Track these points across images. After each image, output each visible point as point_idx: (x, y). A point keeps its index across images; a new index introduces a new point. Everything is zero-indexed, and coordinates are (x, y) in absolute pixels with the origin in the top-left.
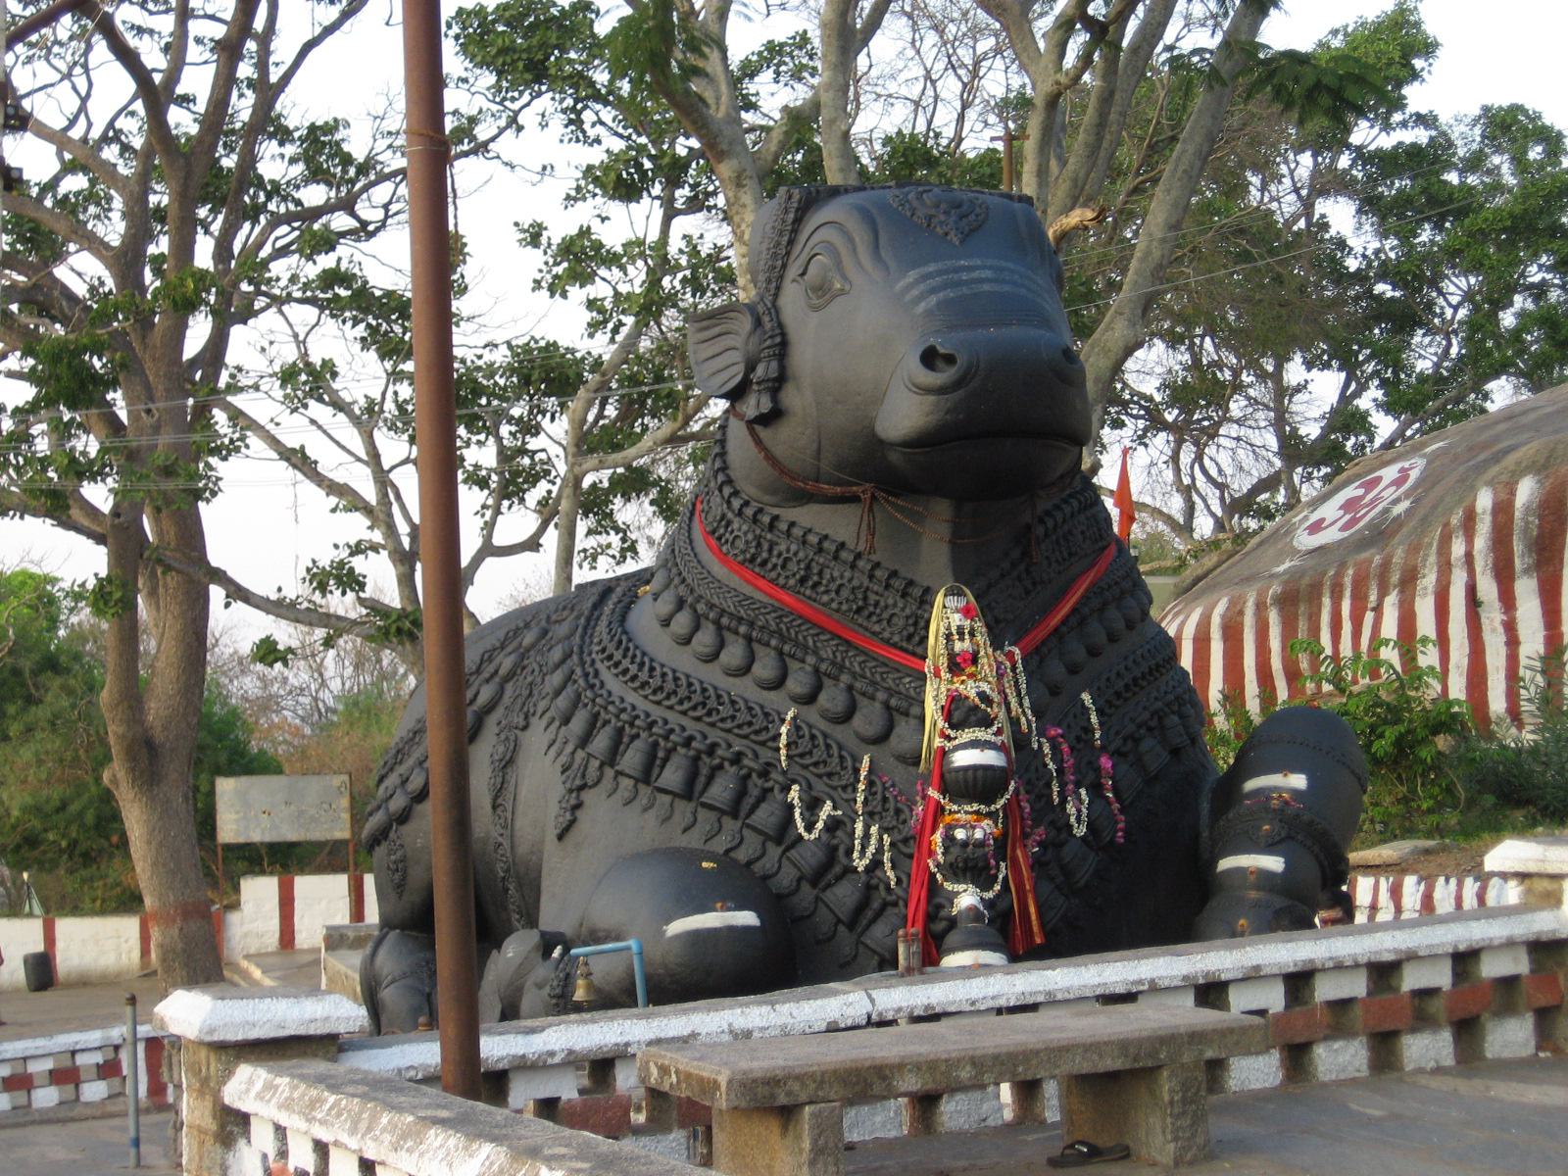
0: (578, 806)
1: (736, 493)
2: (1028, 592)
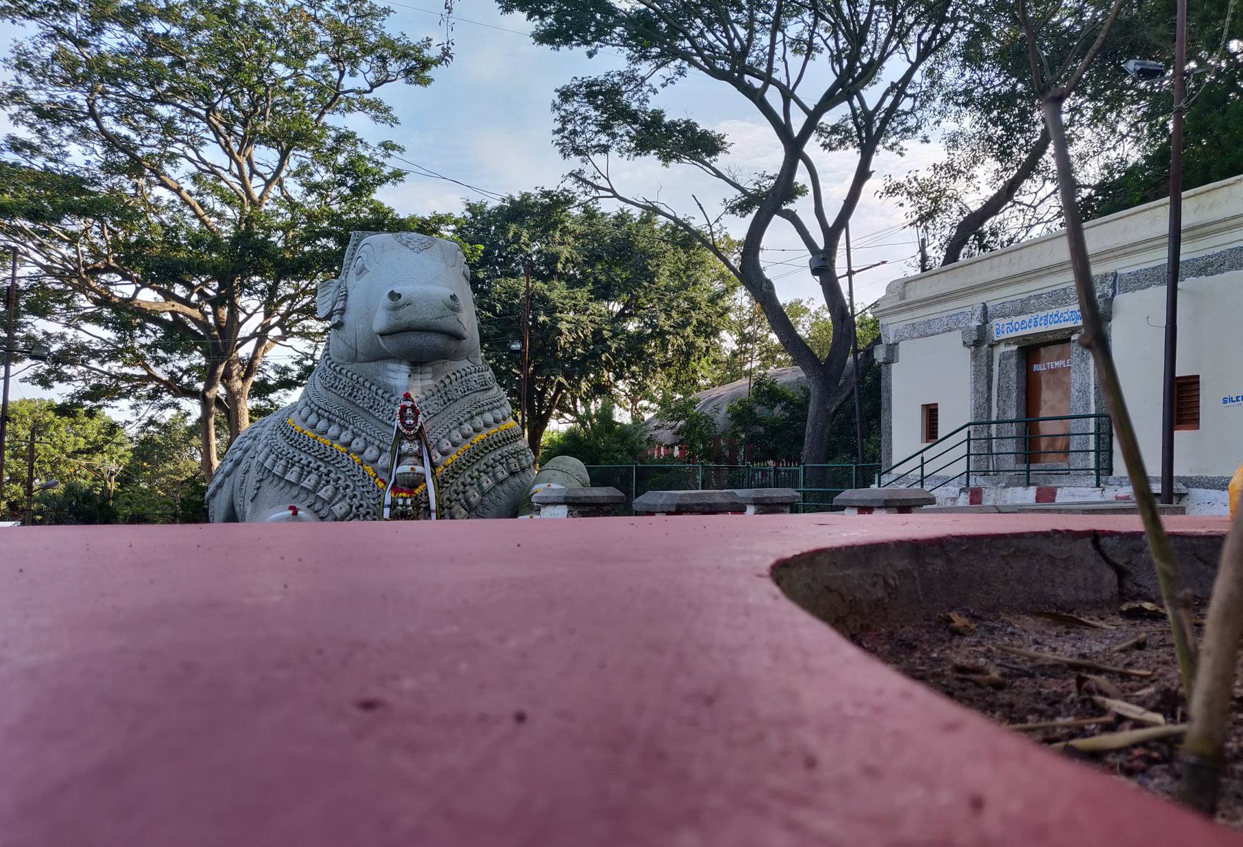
0: (258, 488)
1: (329, 359)
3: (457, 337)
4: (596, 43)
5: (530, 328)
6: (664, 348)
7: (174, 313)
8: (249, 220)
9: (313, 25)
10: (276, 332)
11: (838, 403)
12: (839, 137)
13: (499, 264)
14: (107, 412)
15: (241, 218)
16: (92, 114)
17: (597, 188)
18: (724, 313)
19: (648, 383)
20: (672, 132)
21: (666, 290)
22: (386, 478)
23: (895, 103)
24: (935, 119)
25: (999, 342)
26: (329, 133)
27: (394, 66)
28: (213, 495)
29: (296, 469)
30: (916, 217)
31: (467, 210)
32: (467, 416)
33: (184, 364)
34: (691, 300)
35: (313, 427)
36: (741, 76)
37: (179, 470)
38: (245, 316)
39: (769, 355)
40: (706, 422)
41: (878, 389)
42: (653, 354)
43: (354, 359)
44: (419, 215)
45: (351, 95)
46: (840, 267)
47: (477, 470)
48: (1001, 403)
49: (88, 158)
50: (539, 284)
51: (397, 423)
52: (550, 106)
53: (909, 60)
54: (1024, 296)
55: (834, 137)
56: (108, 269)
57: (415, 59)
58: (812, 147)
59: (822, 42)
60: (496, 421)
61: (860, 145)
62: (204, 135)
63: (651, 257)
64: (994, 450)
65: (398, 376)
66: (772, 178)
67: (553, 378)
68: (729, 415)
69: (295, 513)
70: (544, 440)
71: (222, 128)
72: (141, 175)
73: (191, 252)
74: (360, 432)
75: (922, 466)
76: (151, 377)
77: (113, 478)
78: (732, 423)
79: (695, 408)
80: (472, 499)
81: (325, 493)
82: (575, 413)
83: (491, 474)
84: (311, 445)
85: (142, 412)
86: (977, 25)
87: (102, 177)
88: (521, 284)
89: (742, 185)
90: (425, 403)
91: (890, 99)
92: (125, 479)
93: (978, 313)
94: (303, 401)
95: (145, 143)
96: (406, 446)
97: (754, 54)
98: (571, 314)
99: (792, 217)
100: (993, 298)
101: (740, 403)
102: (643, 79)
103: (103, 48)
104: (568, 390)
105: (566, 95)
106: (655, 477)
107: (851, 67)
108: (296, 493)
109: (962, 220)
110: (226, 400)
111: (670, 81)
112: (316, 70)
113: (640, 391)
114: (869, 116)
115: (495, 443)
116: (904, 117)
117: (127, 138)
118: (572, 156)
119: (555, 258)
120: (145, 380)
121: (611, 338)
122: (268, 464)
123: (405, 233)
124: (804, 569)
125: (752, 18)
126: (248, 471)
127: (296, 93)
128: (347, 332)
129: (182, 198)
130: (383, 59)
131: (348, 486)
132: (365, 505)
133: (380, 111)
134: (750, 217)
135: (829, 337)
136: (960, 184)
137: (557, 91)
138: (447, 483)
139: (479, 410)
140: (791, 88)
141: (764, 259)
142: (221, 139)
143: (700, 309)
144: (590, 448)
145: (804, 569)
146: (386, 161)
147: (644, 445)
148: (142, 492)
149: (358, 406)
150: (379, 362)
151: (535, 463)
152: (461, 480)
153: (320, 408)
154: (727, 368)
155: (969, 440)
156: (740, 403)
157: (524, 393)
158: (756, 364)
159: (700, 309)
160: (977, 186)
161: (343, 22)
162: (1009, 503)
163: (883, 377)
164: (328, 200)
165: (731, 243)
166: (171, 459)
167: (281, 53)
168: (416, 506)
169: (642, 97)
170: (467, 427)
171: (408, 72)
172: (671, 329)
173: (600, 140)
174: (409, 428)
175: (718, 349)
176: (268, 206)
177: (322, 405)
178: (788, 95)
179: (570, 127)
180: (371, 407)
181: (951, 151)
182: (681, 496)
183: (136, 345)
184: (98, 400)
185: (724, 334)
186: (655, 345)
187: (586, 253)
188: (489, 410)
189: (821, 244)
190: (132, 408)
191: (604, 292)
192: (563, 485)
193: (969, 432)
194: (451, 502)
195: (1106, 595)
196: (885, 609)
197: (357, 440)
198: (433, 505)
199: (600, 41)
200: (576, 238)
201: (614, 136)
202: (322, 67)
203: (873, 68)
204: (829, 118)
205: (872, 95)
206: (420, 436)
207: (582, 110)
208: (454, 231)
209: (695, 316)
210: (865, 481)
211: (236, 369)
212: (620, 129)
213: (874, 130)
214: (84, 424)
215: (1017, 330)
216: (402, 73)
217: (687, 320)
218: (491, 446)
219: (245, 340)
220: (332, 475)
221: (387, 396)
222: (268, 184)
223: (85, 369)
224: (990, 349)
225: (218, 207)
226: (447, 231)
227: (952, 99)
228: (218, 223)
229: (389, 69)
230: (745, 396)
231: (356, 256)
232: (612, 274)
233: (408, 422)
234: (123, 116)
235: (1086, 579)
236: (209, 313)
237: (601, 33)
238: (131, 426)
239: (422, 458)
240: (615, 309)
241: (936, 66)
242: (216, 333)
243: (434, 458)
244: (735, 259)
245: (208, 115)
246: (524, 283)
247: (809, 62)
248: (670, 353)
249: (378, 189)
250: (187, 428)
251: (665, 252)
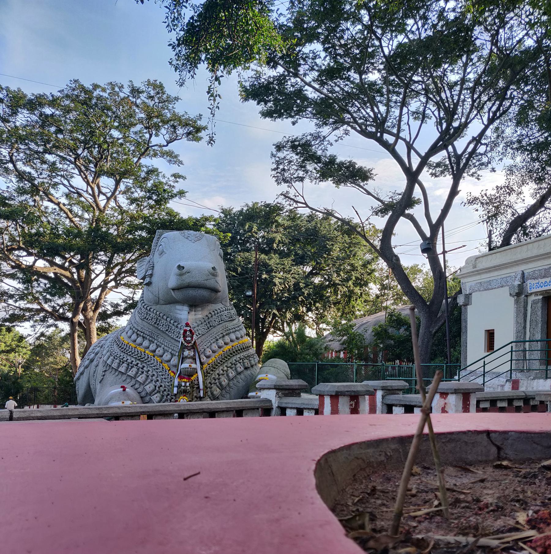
0: (104, 375)
1: (143, 303)
2: (208, 328)
3: (216, 291)
4: (297, 117)
5: (258, 281)
6: (336, 293)
7: (55, 274)
8: (98, 221)
9: (134, 108)
10: (113, 284)
11: (437, 328)
12: (441, 169)
13: (240, 244)
14: (17, 329)
15: (93, 219)
16: (11, 161)
17: (297, 202)
18: (371, 273)
19: (326, 314)
20: (341, 168)
21: (337, 259)
22: (175, 370)
23: (475, 149)
24: (499, 158)
25: (531, 294)
26: (142, 169)
27: (180, 131)
28: (78, 379)
29: (125, 365)
30: (486, 217)
31: (221, 212)
32: (221, 335)
33: (60, 302)
34: (352, 265)
35: (135, 341)
36: (382, 135)
37: (56, 362)
38: (95, 275)
39: (398, 299)
40: (359, 338)
41: (460, 319)
42: (329, 297)
43: (157, 303)
44: (194, 217)
45: (156, 148)
46: (439, 249)
47: (226, 366)
48: (532, 329)
49: (8, 185)
50: (263, 256)
51: (182, 339)
52: (270, 155)
53: (483, 123)
54: (546, 267)
55: (437, 169)
56: (19, 248)
57: (192, 127)
58: (425, 176)
59: (431, 113)
60: (237, 338)
61: (453, 174)
62: (73, 171)
63: (328, 240)
64: (527, 358)
65: (182, 313)
66: (400, 194)
67: (270, 310)
68: (373, 334)
69: (124, 390)
70: (265, 346)
71: (83, 168)
72: (38, 194)
73: (65, 239)
74: (160, 345)
75: (484, 366)
76: (42, 310)
77: (20, 366)
78: (375, 338)
79: (353, 329)
80: (223, 383)
81: (141, 379)
82: (283, 331)
83: (234, 369)
84: (133, 351)
85: (37, 330)
86: (526, 101)
87: (15, 195)
88: (252, 256)
89: (382, 199)
90: (197, 328)
91: (472, 146)
92: (27, 367)
93: (519, 276)
94: (129, 327)
95: (40, 177)
96: (186, 353)
97: (391, 121)
98: (282, 273)
99: (411, 218)
100: (528, 268)
101: (380, 326)
102: (324, 137)
103: (18, 124)
104: (279, 317)
105: (279, 147)
106: (329, 370)
107: (448, 128)
108: (125, 378)
109: (513, 219)
110: (84, 323)
111: (341, 138)
112: (136, 133)
113: (320, 318)
114: (458, 157)
115: (236, 351)
116: (480, 157)
117: (30, 173)
118: (283, 183)
119: (272, 240)
120: (38, 311)
121: (305, 287)
122: (109, 362)
123: (186, 231)
124: (345, 451)
125: (389, 100)
126: (98, 365)
127: (124, 146)
128: (154, 287)
129: (60, 207)
130: (174, 127)
131: (154, 375)
132: (163, 386)
133: (172, 157)
134: (387, 217)
135: (432, 286)
136: (513, 198)
137: (274, 145)
138: (209, 373)
139: (227, 332)
140: (411, 143)
141: (394, 241)
142: (82, 174)
143: (357, 270)
144: (292, 352)
145: (345, 451)
146: (175, 185)
147: (323, 351)
148: (36, 374)
149: (159, 330)
150: (172, 305)
151: (259, 362)
152: (217, 372)
153: (138, 331)
154: (373, 305)
155: (512, 351)
156: (380, 326)
157: (253, 319)
158: (389, 303)
159: (357, 270)
160: (523, 198)
161: (151, 106)
162: (535, 389)
163: (462, 313)
164: (142, 207)
165: (376, 231)
166: (52, 355)
167: (116, 124)
168: (192, 387)
169: (323, 148)
170: (221, 342)
171: (188, 134)
172: (340, 283)
173: (298, 174)
174: (188, 342)
175: (368, 294)
176: (108, 212)
177: (139, 329)
178: (410, 147)
179: (281, 167)
180: (167, 330)
181: (508, 177)
182: (338, 386)
183: (34, 291)
184: (13, 322)
185: (371, 285)
186: (331, 292)
187: (290, 238)
188: (233, 332)
189: (428, 234)
190: (32, 327)
191: (300, 260)
192: (274, 375)
193: (512, 347)
195: (491, 458)
196: (385, 465)
197: (159, 349)
198: (201, 387)
199: (299, 115)
200: (285, 229)
201: (307, 172)
202: (140, 131)
203: (460, 131)
204: (435, 159)
205: (460, 144)
206: (194, 347)
207: (288, 157)
208: (214, 225)
209: (354, 274)
210: (451, 374)
211: (90, 305)
212: (310, 166)
213: (462, 165)
214: (4, 335)
215: (542, 287)
216: (185, 135)
217: (350, 277)
218: (234, 352)
219: (95, 289)
220: (145, 369)
221: (176, 324)
222: (108, 199)
223: (6, 305)
224: (525, 298)
225: (80, 213)
226: (210, 226)
227: (509, 146)
228: (80, 221)
229: (178, 132)
230: (383, 323)
231: (159, 244)
232: (306, 250)
233: (187, 339)
234: (28, 161)
235: (482, 451)
236: (75, 273)
237: (300, 111)
238: (31, 337)
239: (195, 359)
240: (307, 270)
241: (500, 126)
242: (78, 284)
243: (202, 359)
244: (377, 243)
245: (75, 161)
246: (254, 255)
247: (423, 124)
248: (339, 296)
249: (170, 201)
250: (61, 338)
251: (337, 237)
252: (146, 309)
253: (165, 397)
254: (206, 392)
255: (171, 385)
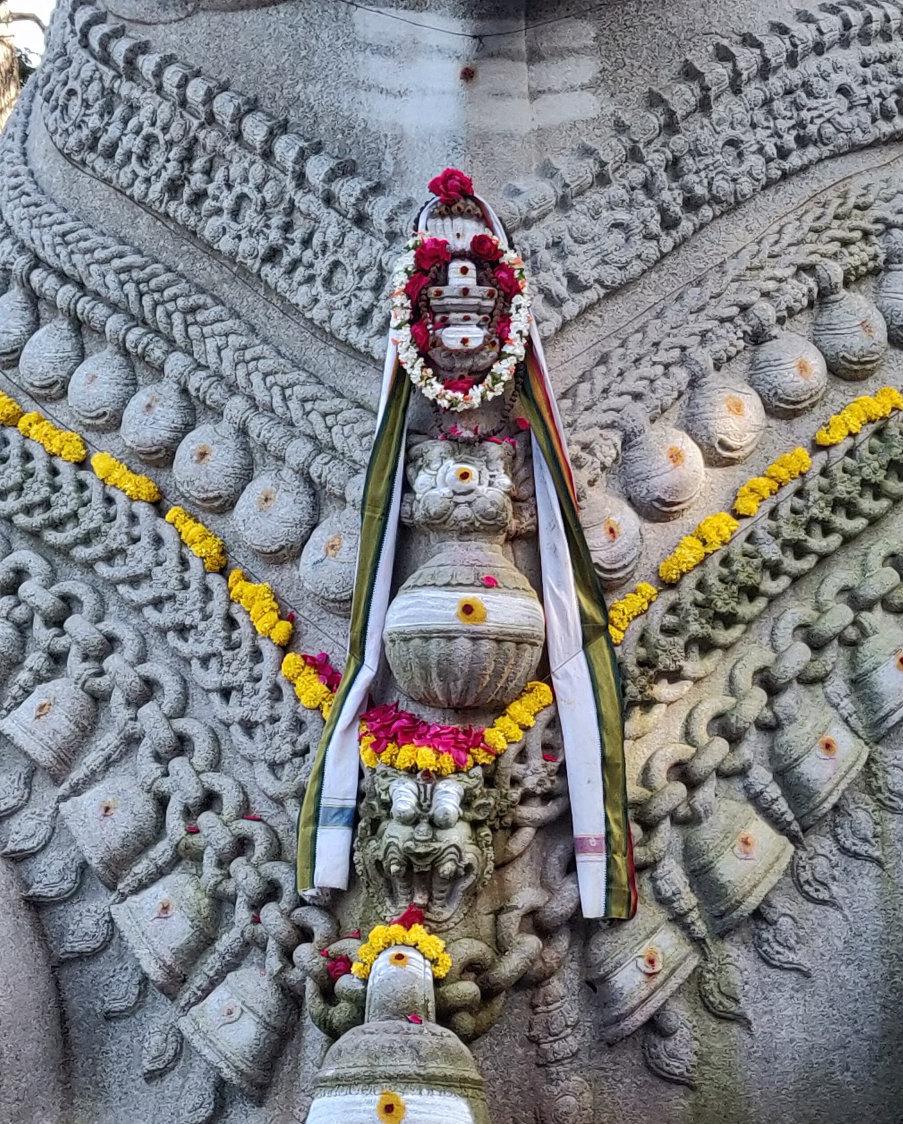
2: (669, 223)
65: (405, 78)
74: (216, 394)
90: (556, 224)
132: (230, 801)
139: (859, 255)
149: (210, 250)
153: (37, 262)
180: (272, 255)
194: (693, 784)
233: (451, 337)
239: (531, 538)
243: (596, 539)
252: (106, 60)
253: (242, 914)
254: (638, 869)
255: (300, 795)
